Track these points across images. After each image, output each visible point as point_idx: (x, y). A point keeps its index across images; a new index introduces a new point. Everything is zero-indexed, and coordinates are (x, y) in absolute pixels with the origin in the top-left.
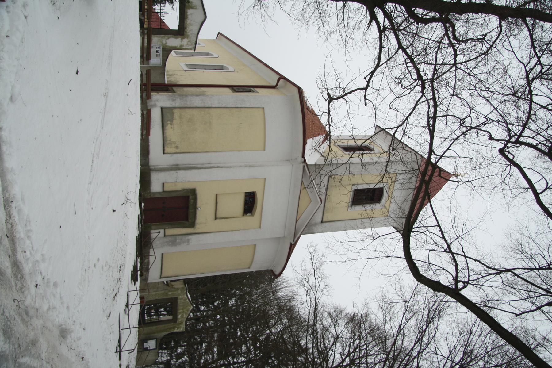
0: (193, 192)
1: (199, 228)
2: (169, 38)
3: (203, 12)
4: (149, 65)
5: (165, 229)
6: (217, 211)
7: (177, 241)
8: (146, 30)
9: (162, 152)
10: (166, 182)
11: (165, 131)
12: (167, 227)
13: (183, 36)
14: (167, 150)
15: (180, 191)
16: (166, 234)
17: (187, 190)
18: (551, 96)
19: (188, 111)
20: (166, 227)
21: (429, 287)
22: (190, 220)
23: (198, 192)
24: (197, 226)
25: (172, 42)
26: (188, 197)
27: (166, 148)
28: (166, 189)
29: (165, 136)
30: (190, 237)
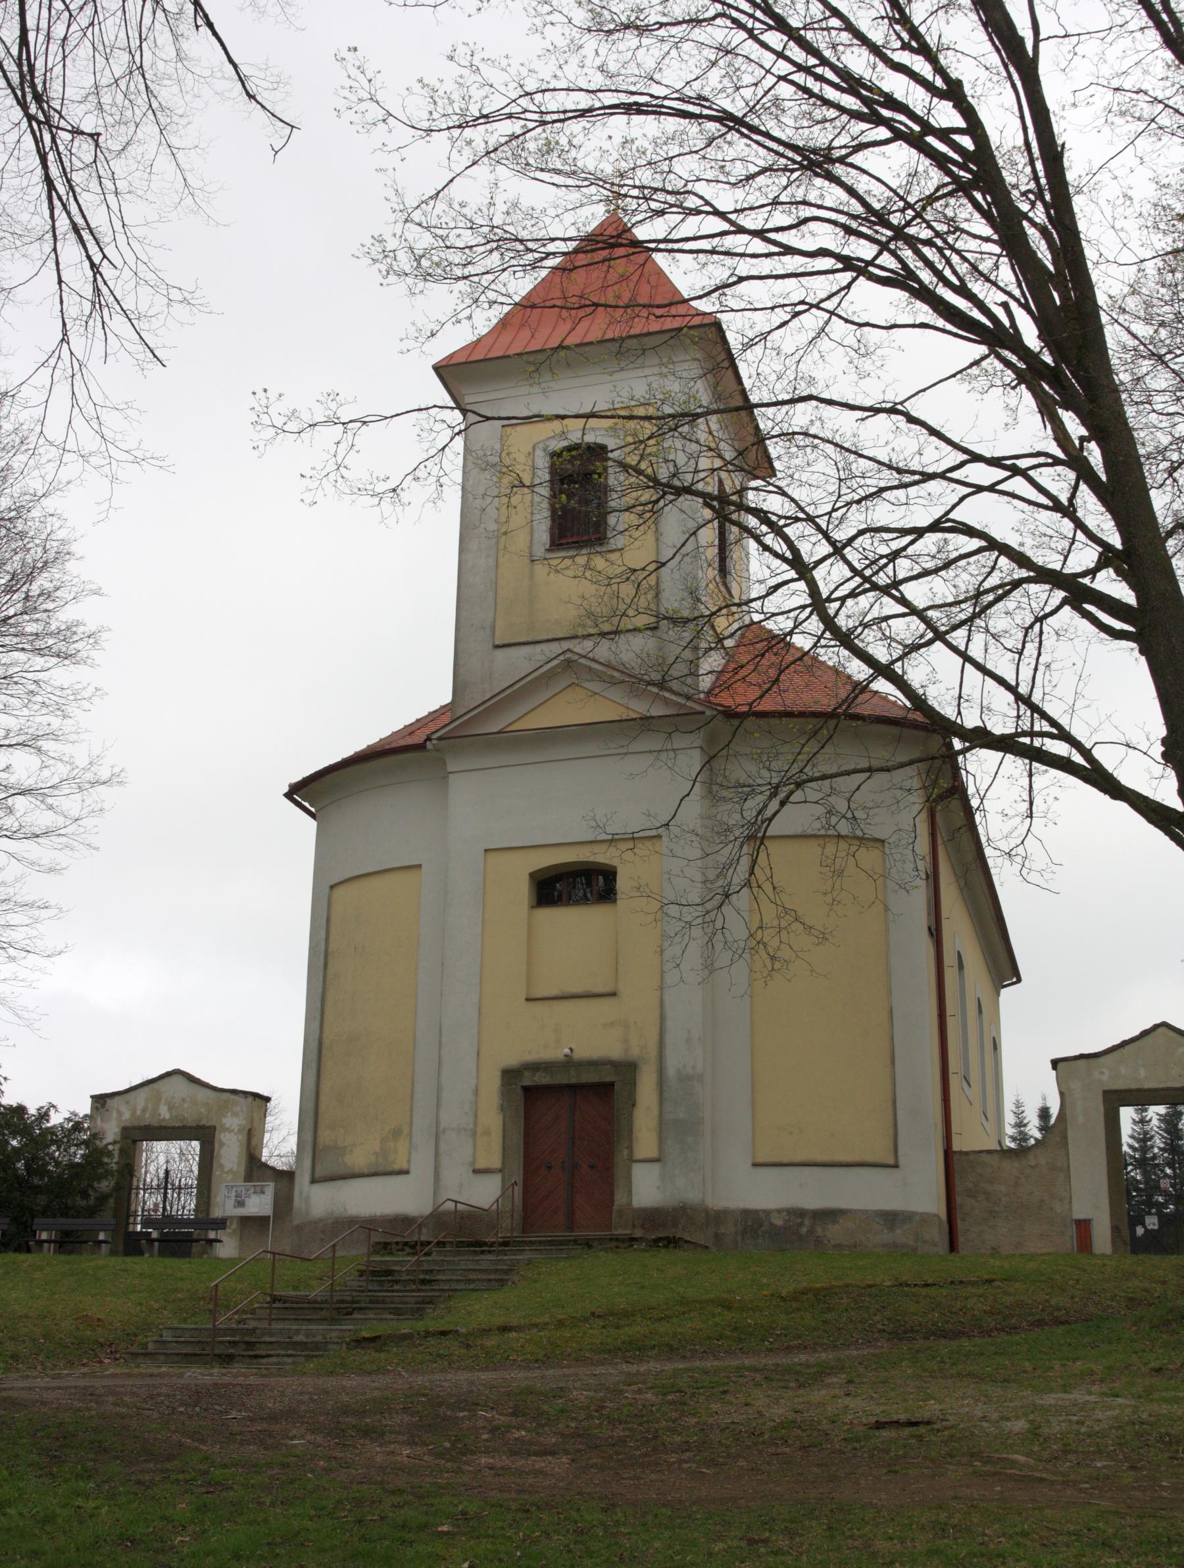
0: (510, 1075)
1: (641, 1045)
2: (221, 1166)
3: (166, 1080)
4: (269, 1217)
5: (632, 1160)
6: (596, 990)
7: (682, 1115)
8: (1135, 1232)
9: (894, 1170)
10: (473, 1162)
11: (356, 1170)
12: (626, 1152)
13: (218, 1128)
14: (401, 1164)
15: (504, 1117)
16: (654, 1153)
17: (502, 1094)
18: (1177, 101)
19: (323, 1107)
20: (626, 1157)
21: (970, 290)
22: (609, 1079)
23: (512, 1059)
24: (635, 1052)
25: (230, 1154)
26: (526, 1089)
27: (396, 1167)
28: (496, 1162)
29: (366, 1171)
30: (671, 1072)
